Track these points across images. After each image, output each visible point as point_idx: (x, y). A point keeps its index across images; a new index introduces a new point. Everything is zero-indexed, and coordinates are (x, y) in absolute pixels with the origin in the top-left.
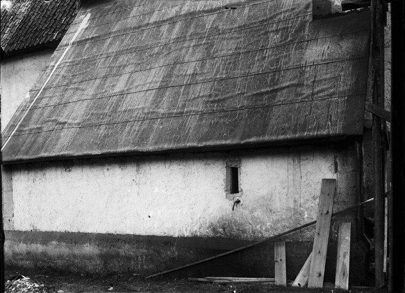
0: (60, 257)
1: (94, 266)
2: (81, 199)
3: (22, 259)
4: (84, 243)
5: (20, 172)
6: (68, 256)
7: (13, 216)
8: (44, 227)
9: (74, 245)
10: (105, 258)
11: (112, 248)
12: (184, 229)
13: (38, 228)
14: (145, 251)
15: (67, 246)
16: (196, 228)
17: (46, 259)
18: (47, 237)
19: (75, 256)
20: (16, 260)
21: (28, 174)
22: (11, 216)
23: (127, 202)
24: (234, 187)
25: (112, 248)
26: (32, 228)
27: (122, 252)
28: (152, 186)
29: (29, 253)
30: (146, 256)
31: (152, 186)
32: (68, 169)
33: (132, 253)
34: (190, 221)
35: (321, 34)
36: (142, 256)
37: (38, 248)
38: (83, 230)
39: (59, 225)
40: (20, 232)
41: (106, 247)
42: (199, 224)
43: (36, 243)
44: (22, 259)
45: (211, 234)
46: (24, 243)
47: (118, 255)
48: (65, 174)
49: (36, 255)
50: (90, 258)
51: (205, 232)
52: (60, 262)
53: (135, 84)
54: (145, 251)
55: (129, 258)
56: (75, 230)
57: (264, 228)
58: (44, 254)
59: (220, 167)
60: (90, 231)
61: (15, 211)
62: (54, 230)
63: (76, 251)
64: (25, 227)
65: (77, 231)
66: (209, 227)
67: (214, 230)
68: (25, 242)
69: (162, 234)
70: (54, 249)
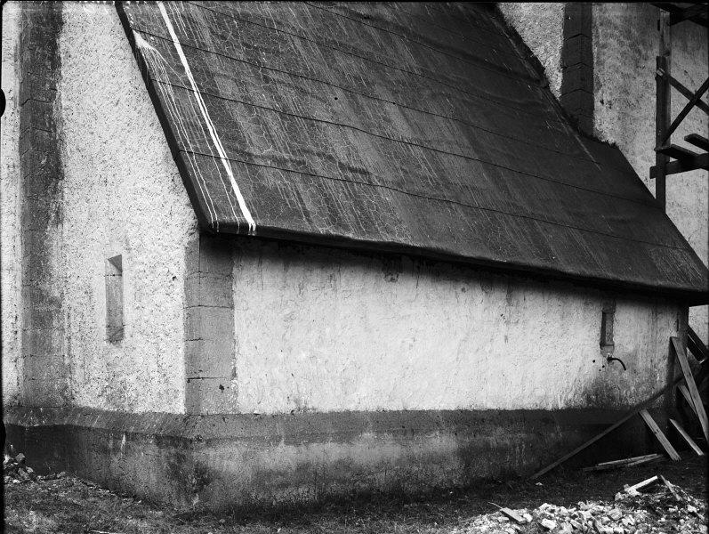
0: (383, 465)
1: (450, 473)
2: (412, 342)
3: (284, 486)
4: (430, 431)
5: (260, 263)
6: (399, 461)
7: (234, 375)
8: (327, 401)
9: (410, 436)
10: (466, 455)
11: (478, 436)
12: (559, 397)
13: (310, 406)
14: (523, 435)
15: (398, 441)
16: (570, 396)
17: (348, 475)
18: (347, 425)
19: (412, 460)
20: (266, 489)
21: (286, 270)
22: (229, 374)
23: (490, 352)
24: (605, 341)
25: (478, 436)
26: (293, 406)
27: (493, 440)
28: (524, 328)
29: (303, 468)
30: (527, 444)
31: (524, 328)
32: (390, 277)
33: (508, 442)
34: (566, 386)
35: (235, 270)
36: (520, 445)
37: (329, 452)
38: (416, 404)
39: (365, 398)
40: (260, 418)
41: (469, 434)
42: (574, 389)
43: (323, 441)
44: (284, 486)
45: (585, 404)
46: (287, 443)
47: (487, 448)
48: (385, 285)
49: (325, 469)
50: (440, 460)
51: (580, 401)
52: (381, 479)
53: (428, 174)
54: (523, 435)
55: (503, 451)
56: (396, 406)
57: (629, 393)
58: (344, 465)
59: (598, 310)
60: (426, 408)
61: (240, 364)
62: (352, 407)
63: (416, 450)
64: (275, 403)
65: (401, 409)
66: (584, 394)
67: (589, 399)
68: (293, 439)
69: (534, 407)
70: (367, 451)
